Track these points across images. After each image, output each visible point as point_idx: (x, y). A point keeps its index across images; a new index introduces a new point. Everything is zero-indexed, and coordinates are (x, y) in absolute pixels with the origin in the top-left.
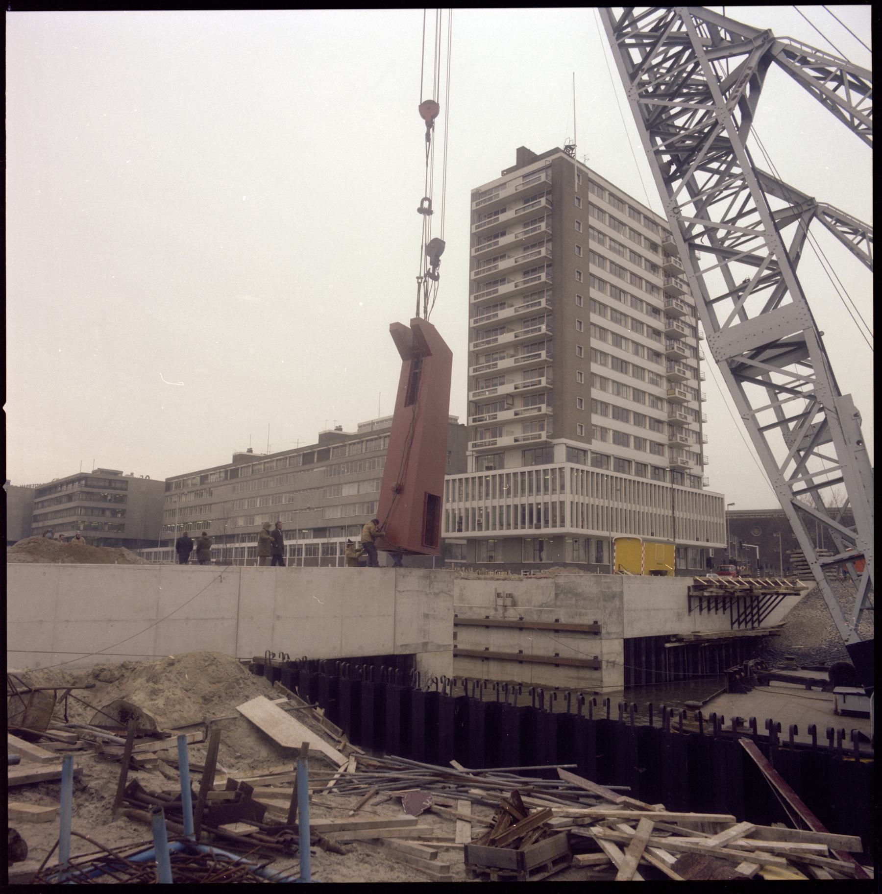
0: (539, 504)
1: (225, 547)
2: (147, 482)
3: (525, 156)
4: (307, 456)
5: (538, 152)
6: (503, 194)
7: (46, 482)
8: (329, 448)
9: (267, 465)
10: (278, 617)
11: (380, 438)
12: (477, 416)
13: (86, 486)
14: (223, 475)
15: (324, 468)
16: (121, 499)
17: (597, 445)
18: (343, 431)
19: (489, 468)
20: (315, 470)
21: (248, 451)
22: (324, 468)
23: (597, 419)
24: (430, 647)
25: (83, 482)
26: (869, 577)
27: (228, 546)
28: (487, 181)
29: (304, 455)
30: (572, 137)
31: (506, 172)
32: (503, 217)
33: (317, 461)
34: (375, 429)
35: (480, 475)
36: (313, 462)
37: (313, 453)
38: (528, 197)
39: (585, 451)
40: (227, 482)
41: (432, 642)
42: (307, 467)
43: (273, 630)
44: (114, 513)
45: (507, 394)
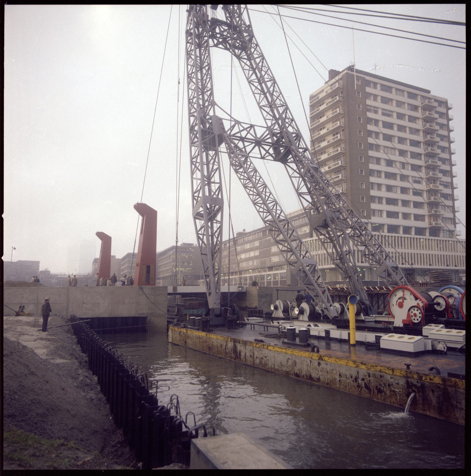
3: (333, 73)
5: (341, 71)
6: (321, 96)
17: (375, 220)
23: (374, 206)
26: (349, 312)
28: (315, 90)
29: (263, 231)
31: (326, 83)
32: (322, 108)
38: (332, 95)
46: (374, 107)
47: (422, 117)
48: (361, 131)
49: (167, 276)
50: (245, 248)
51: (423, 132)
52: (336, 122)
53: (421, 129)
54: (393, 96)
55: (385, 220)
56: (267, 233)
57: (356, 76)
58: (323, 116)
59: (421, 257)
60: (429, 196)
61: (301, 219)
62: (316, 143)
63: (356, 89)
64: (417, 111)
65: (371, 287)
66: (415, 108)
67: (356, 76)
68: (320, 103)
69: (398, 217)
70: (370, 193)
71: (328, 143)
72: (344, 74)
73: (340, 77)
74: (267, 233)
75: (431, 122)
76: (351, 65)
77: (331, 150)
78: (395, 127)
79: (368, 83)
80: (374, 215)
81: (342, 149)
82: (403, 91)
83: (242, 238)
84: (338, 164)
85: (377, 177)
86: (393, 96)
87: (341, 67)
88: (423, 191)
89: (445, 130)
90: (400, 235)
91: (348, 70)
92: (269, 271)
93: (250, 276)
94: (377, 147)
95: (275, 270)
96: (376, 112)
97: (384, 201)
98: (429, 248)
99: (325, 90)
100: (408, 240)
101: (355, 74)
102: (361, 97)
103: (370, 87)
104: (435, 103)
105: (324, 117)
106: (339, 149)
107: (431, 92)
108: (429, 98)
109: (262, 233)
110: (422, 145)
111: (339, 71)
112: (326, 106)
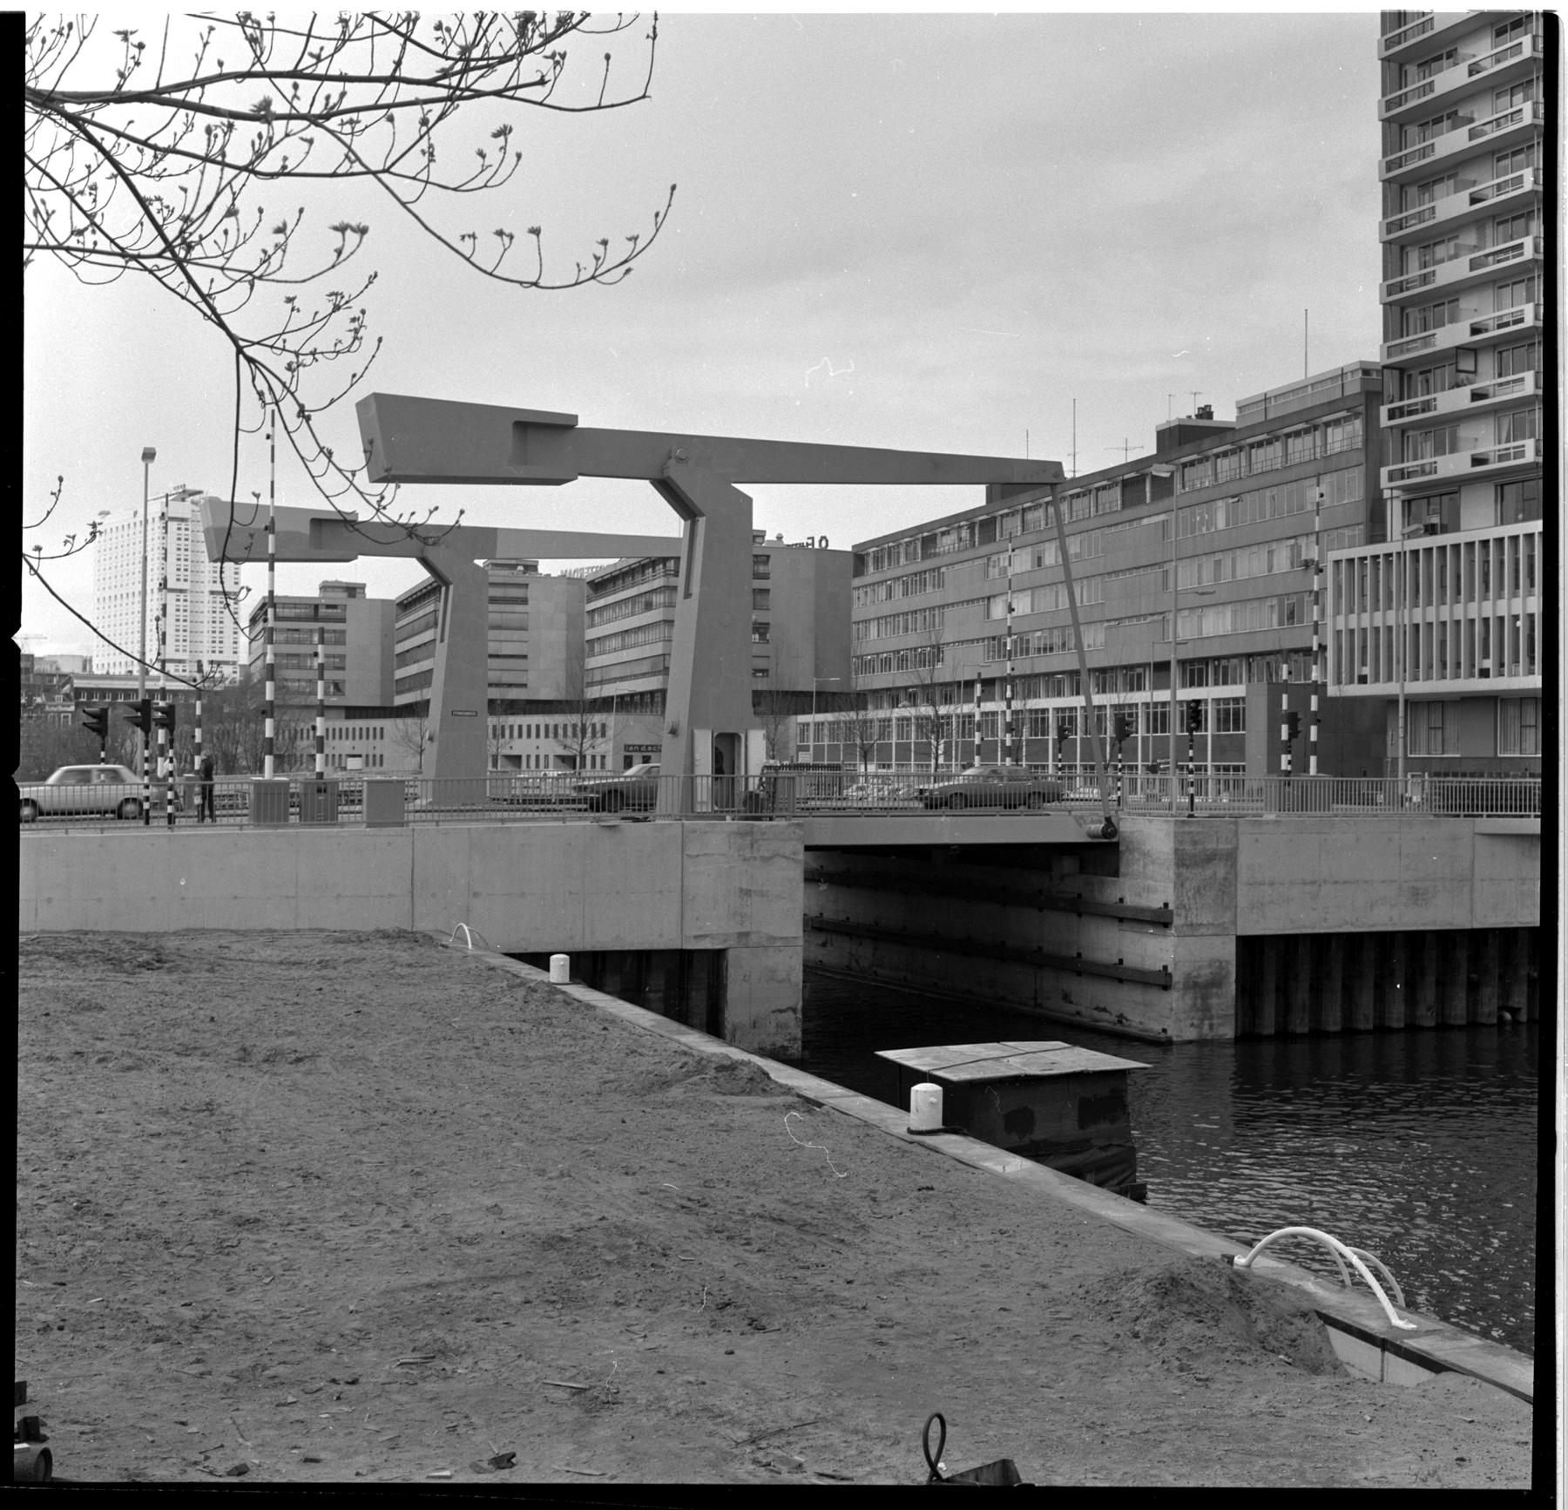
0: (1516, 618)
1: (952, 707)
10: (476, 895)
12: (1406, 402)
14: (965, 533)
15: (1162, 517)
18: (1216, 417)
19: (1431, 530)
20: (1145, 521)
21: (1199, 416)
24: (754, 938)
27: (943, 710)
29: (1126, 484)
33: (1153, 499)
34: (1271, 416)
36: (1142, 501)
37: (1140, 480)
40: (970, 554)
41: (758, 932)
42: (1130, 513)
43: (468, 910)
45: (1458, 348)
49: (642, 694)
56: (1148, 495)
61: (1094, 492)
62: (1413, 191)
65: (470, 946)
71: (1471, 74)
74: (1148, 495)
89: (54, 681)
93: (1063, 710)
100: (616, 797)
109: (1118, 490)
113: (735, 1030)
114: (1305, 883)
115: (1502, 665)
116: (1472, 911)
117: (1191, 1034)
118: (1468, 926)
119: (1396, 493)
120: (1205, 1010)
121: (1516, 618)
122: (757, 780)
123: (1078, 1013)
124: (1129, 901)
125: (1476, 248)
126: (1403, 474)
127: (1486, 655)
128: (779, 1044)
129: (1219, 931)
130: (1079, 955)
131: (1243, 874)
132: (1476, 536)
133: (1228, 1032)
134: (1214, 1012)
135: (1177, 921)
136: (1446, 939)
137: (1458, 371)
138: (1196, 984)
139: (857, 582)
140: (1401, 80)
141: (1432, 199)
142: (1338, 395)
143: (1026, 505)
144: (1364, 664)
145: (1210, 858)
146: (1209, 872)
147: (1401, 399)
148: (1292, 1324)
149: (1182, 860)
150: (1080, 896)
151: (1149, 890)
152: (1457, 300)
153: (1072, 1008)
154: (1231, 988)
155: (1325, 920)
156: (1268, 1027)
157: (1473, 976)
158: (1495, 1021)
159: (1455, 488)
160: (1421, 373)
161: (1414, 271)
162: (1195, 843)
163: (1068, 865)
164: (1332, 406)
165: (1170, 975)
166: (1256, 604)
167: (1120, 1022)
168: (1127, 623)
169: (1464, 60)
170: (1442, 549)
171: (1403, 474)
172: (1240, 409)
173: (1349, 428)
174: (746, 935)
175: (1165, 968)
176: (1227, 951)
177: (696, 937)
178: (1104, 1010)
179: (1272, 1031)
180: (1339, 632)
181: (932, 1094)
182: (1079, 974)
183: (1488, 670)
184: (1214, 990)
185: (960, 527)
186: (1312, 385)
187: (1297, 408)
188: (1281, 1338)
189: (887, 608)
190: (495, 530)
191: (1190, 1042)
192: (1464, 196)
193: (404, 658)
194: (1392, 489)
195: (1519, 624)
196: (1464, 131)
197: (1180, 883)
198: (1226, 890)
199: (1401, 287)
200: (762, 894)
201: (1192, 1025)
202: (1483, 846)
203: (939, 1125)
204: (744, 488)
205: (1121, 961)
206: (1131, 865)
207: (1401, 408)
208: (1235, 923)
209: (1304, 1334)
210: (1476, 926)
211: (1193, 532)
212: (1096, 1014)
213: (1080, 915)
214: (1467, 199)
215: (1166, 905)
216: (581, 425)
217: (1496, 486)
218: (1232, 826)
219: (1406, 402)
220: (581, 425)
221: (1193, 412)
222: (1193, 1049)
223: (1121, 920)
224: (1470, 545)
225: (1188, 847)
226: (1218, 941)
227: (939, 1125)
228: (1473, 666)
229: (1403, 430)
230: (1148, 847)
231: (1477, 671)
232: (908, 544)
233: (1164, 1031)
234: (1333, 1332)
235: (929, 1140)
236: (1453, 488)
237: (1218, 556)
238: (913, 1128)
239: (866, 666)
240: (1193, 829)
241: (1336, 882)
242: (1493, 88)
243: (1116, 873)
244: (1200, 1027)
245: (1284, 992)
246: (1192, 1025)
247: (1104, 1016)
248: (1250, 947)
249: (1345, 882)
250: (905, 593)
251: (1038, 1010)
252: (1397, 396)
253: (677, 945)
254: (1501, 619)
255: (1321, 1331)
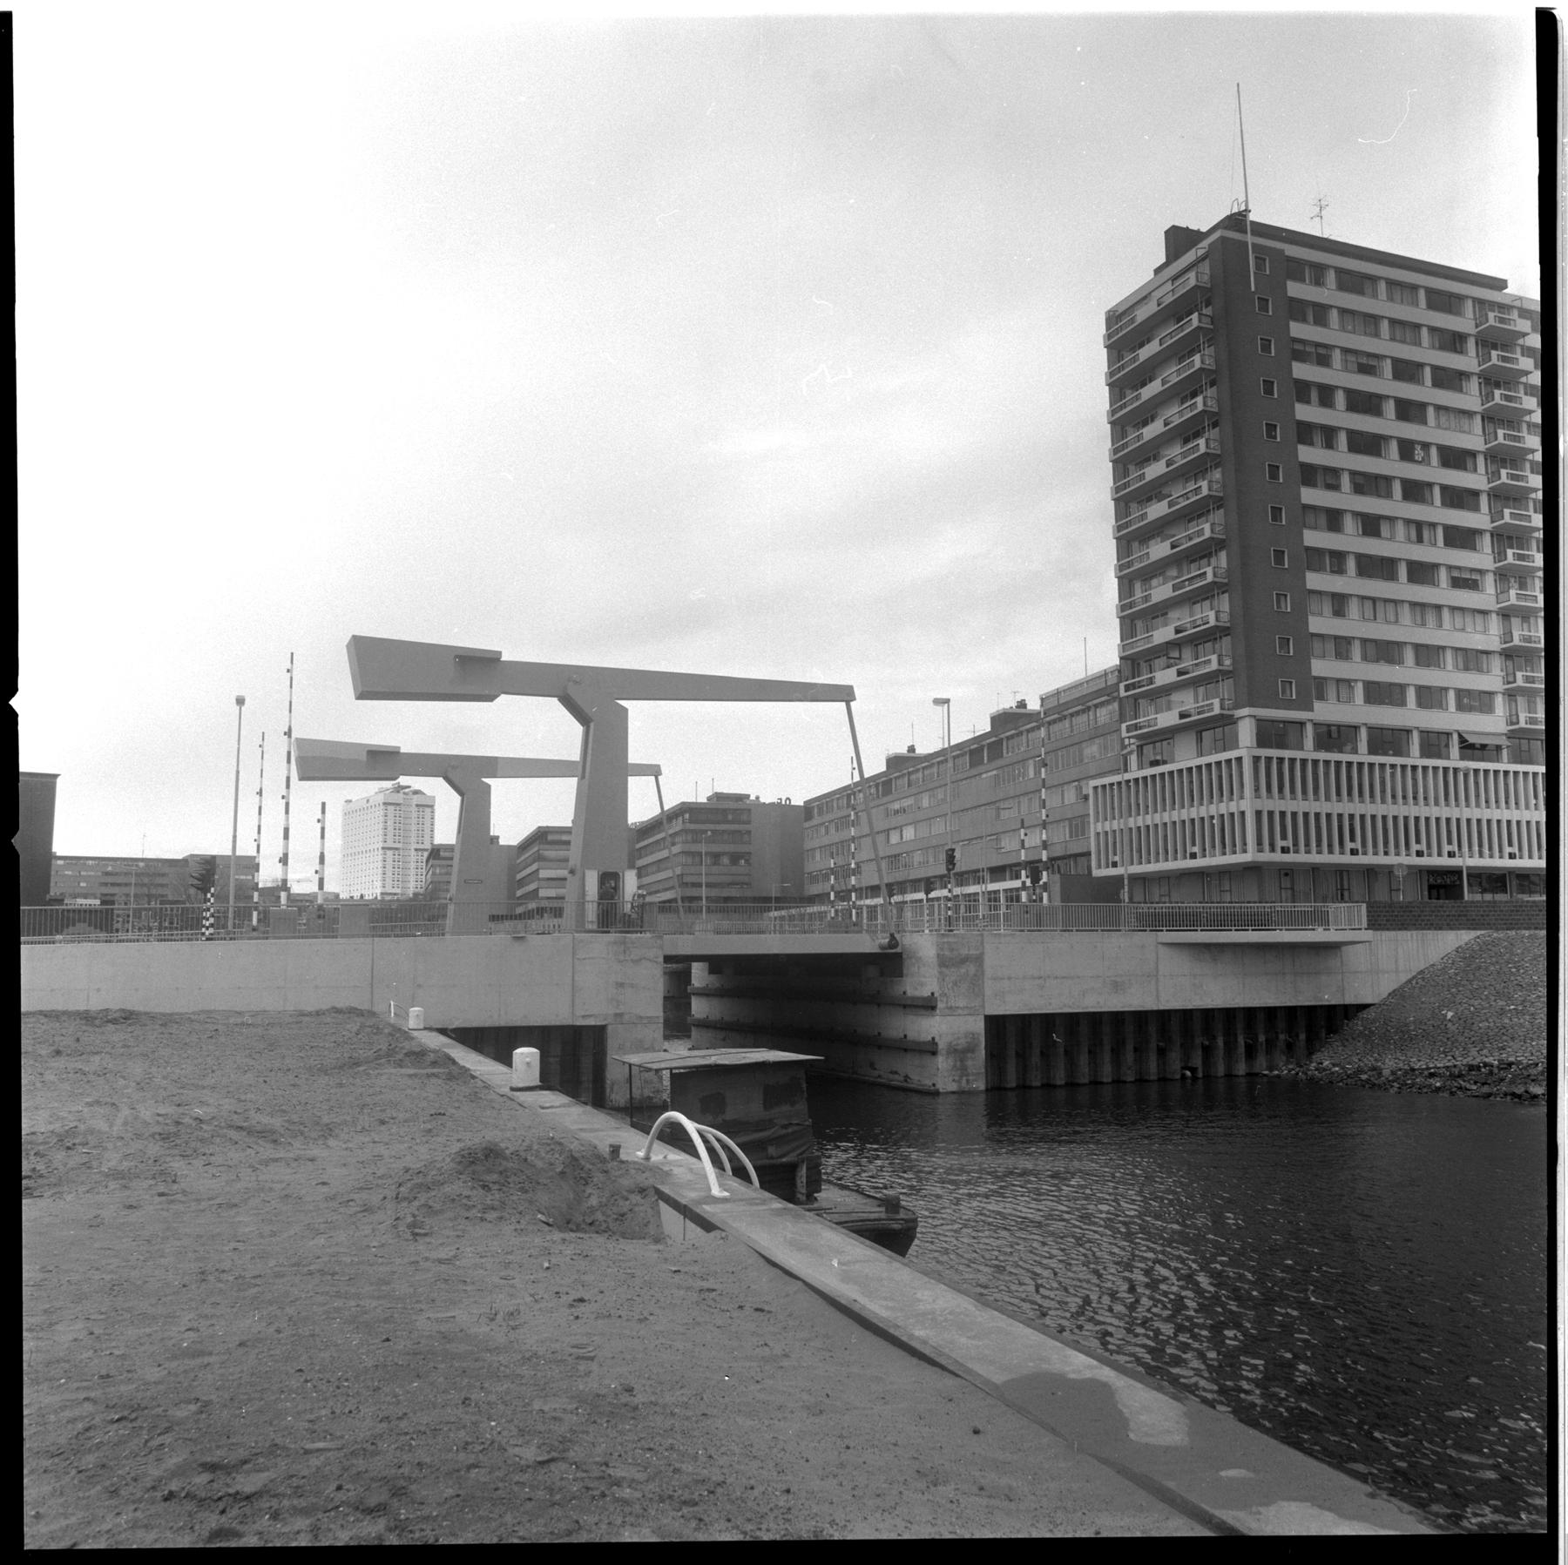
0: (1212, 817)
2: (782, 809)
3: (1179, 239)
4: (976, 752)
5: (1204, 229)
6: (1142, 314)
7: (646, 819)
8: (984, 746)
9: (926, 772)
11: (1065, 717)
12: (1137, 679)
13: (691, 821)
15: (995, 772)
16: (738, 836)
17: (1327, 711)
19: (1155, 763)
20: (984, 776)
21: (909, 751)
22: (995, 772)
24: (626, 1017)
25: (687, 816)
29: (972, 752)
30: (1242, 198)
31: (1157, 271)
33: (989, 760)
34: (1061, 701)
35: (1153, 773)
36: (981, 762)
37: (980, 749)
38: (1177, 311)
39: (1302, 724)
42: (974, 772)
44: (735, 858)
45: (1167, 643)
46: (1318, 345)
47: (1477, 370)
48: (1275, 426)
50: (912, 1035)
51: (1486, 459)
52: (1192, 398)
53: (1482, 488)
54: (1379, 304)
55: (1358, 712)
56: (986, 758)
57: (1254, 245)
58: (1151, 381)
59: (1480, 833)
60: (1499, 547)
62: (1135, 545)
63: (1253, 289)
64: (1476, 509)
66: (1454, 342)
67: (1254, 245)
68: (1142, 335)
69: (1403, 703)
70: (1302, 540)
71: (1168, 466)
72: (1213, 242)
73: (1201, 253)
74: (986, 758)
75: (1506, 346)
76: (1235, 210)
77: (1175, 451)
78: (1390, 408)
79: (1296, 269)
80: (1321, 697)
81: (1215, 486)
82: (1414, 288)
83: (903, 775)
84: (1201, 532)
85: (1333, 572)
86: (1379, 304)
87: (1203, 219)
88: (1481, 572)
90: (1409, 762)
91: (1226, 228)
92: (992, 881)
94: (1328, 477)
95: (1011, 879)
96: (1324, 361)
97: (1351, 564)
98: (1507, 802)
99: (1158, 294)
101: (1250, 239)
102: (1268, 273)
103: (1302, 280)
104: (1519, 321)
105: (1153, 383)
106: (1204, 484)
107: (1509, 284)
108: (1503, 307)
109: (967, 757)
110: (1480, 460)
111: (1198, 232)
112: (1159, 348)
113: (613, 1084)
114: (1033, 978)
115: (1204, 850)
116: (1158, 997)
117: (953, 1087)
118: (1155, 1008)
119: (1132, 741)
120: (963, 1070)
121: (1212, 817)
122: (629, 906)
123: (879, 1076)
124: (909, 993)
125: (1177, 577)
126: (1136, 727)
127: (1194, 844)
128: (646, 1095)
129: (972, 1012)
130: (879, 1034)
131: (989, 972)
132: (1183, 765)
133: (981, 1085)
134: (969, 1071)
135: (940, 1005)
136: (1141, 1018)
137: (1169, 658)
138: (956, 1050)
139: (807, 825)
140: (1126, 473)
141: (1148, 548)
142: (1104, 685)
143: (911, 770)
144: (1115, 854)
145: (964, 960)
146: (963, 971)
147: (1134, 678)
148: (627, 1199)
149: (943, 962)
150: (879, 992)
151: (922, 984)
152: (1166, 614)
153: (876, 1073)
154: (982, 1053)
155: (1050, 1004)
156: (1012, 1080)
157: (1161, 1044)
158: (1178, 1077)
159: (1170, 736)
160: (1146, 662)
161: (1139, 594)
162: (952, 950)
163: (872, 971)
164: (1098, 693)
165: (936, 1044)
166: (1055, 825)
167: (906, 1081)
168: (974, 842)
169: (1163, 457)
170: (1162, 775)
171: (1136, 727)
172: (1042, 700)
173: (1110, 707)
174: (620, 1015)
175: (933, 1039)
176: (979, 1026)
177: (583, 1017)
178: (896, 1073)
179: (1014, 1085)
180: (1098, 834)
181: (532, 1053)
182: (880, 1047)
183: (1195, 854)
184: (969, 1055)
185: (870, 787)
186: (1087, 682)
187: (1077, 695)
188: (610, 1212)
189: (826, 841)
190: (496, 758)
191: (953, 1093)
192: (1167, 544)
193: (522, 883)
194: (1129, 738)
195: (1214, 821)
196: (1165, 502)
197: (942, 978)
198: (976, 984)
199: (1131, 605)
200: (632, 986)
201: (954, 1080)
202: (1163, 951)
203: (537, 1083)
204: (623, 703)
205: (905, 1036)
206: (910, 968)
207: (1134, 683)
208: (983, 1006)
209: (636, 1209)
210: (1162, 1008)
211: (1014, 780)
212: (891, 1076)
213: (879, 1005)
214: (1169, 546)
215: (933, 994)
216: (503, 659)
217: (1197, 732)
218: (980, 938)
219: (1137, 679)
220: (503, 659)
221: (1014, 705)
222: (953, 1097)
223: (905, 1006)
224: (1180, 771)
225: (947, 953)
226: (971, 1019)
227: (537, 1083)
228: (1185, 851)
229: (1136, 698)
230: (921, 954)
231: (1188, 855)
232: (838, 799)
233: (934, 1085)
234: (663, 1206)
235: (522, 1096)
236: (1169, 734)
237: (1030, 796)
238: (514, 1086)
239: (814, 879)
240: (950, 940)
241: (1056, 978)
242: (1183, 475)
243: (901, 975)
244: (959, 1082)
245: (1022, 1056)
246: (954, 1080)
247: (896, 1077)
248: (997, 1025)
249: (1064, 978)
250: (837, 830)
251: (855, 1076)
252: (1130, 676)
253: (569, 1022)
254: (1202, 819)
255: (655, 1207)
